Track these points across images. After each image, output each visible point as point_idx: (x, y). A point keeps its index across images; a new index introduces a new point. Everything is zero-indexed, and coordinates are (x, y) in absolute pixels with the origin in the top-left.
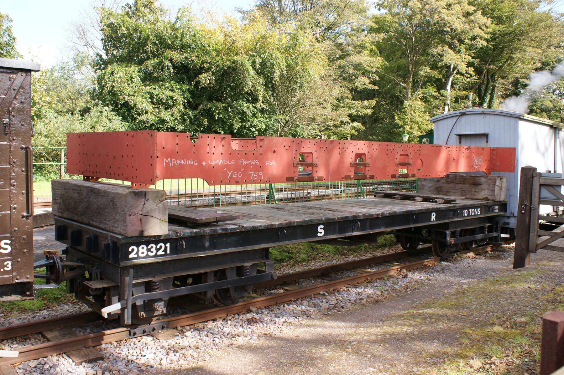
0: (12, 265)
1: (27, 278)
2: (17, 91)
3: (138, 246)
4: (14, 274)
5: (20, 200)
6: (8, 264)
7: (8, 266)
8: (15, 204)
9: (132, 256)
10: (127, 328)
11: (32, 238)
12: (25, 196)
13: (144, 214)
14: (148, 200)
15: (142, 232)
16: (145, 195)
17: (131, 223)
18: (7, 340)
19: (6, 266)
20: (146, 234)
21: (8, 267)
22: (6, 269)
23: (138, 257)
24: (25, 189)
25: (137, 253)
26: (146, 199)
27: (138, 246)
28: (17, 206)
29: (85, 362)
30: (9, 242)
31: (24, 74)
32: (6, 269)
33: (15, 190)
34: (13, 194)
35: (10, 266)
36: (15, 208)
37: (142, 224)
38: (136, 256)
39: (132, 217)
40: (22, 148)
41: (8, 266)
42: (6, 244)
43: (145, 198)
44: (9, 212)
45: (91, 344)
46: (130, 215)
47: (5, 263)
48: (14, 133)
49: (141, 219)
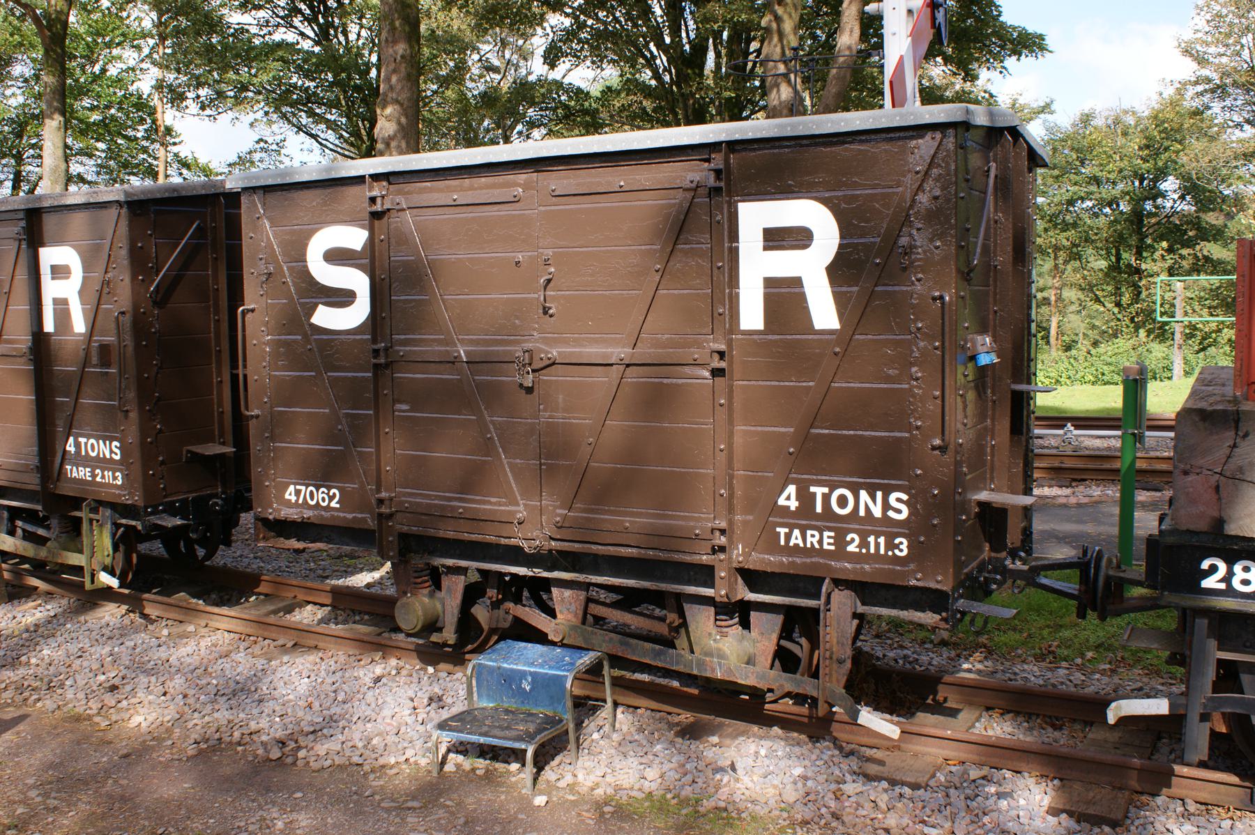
0: (908, 547)
1: (938, 582)
2: (923, 173)
3: (1230, 562)
4: (912, 566)
5: (929, 410)
6: (901, 543)
7: (901, 547)
8: (919, 418)
9: (1210, 583)
10: (1241, 779)
11: (1133, 497)
12: (939, 402)
13: (1228, 474)
14: (1246, 435)
15: (1220, 523)
16: (1237, 422)
17: (1188, 494)
18: (1017, 713)
19: (897, 546)
20: (1232, 529)
21: (901, 550)
22: (897, 552)
23: (1230, 592)
24: (940, 388)
25: (1227, 579)
26: (1240, 433)
27: (1230, 562)
28: (924, 422)
29: (1071, 814)
30: (905, 497)
31: (938, 135)
32: (897, 552)
33: (919, 388)
34: (914, 396)
35: (904, 547)
36: (918, 428)
37: (1219, 499)
38: (1222, 586)
39: (1190, 478)
40: (934, 299)
41: (901, 547)
42: (899, 500)
43: (1237, 429)
44: (229, 450)
45: (1134, 784)
46: (1186, 473)
47: (897, 541)
48: (919, 266)
49: (1217, 488)
